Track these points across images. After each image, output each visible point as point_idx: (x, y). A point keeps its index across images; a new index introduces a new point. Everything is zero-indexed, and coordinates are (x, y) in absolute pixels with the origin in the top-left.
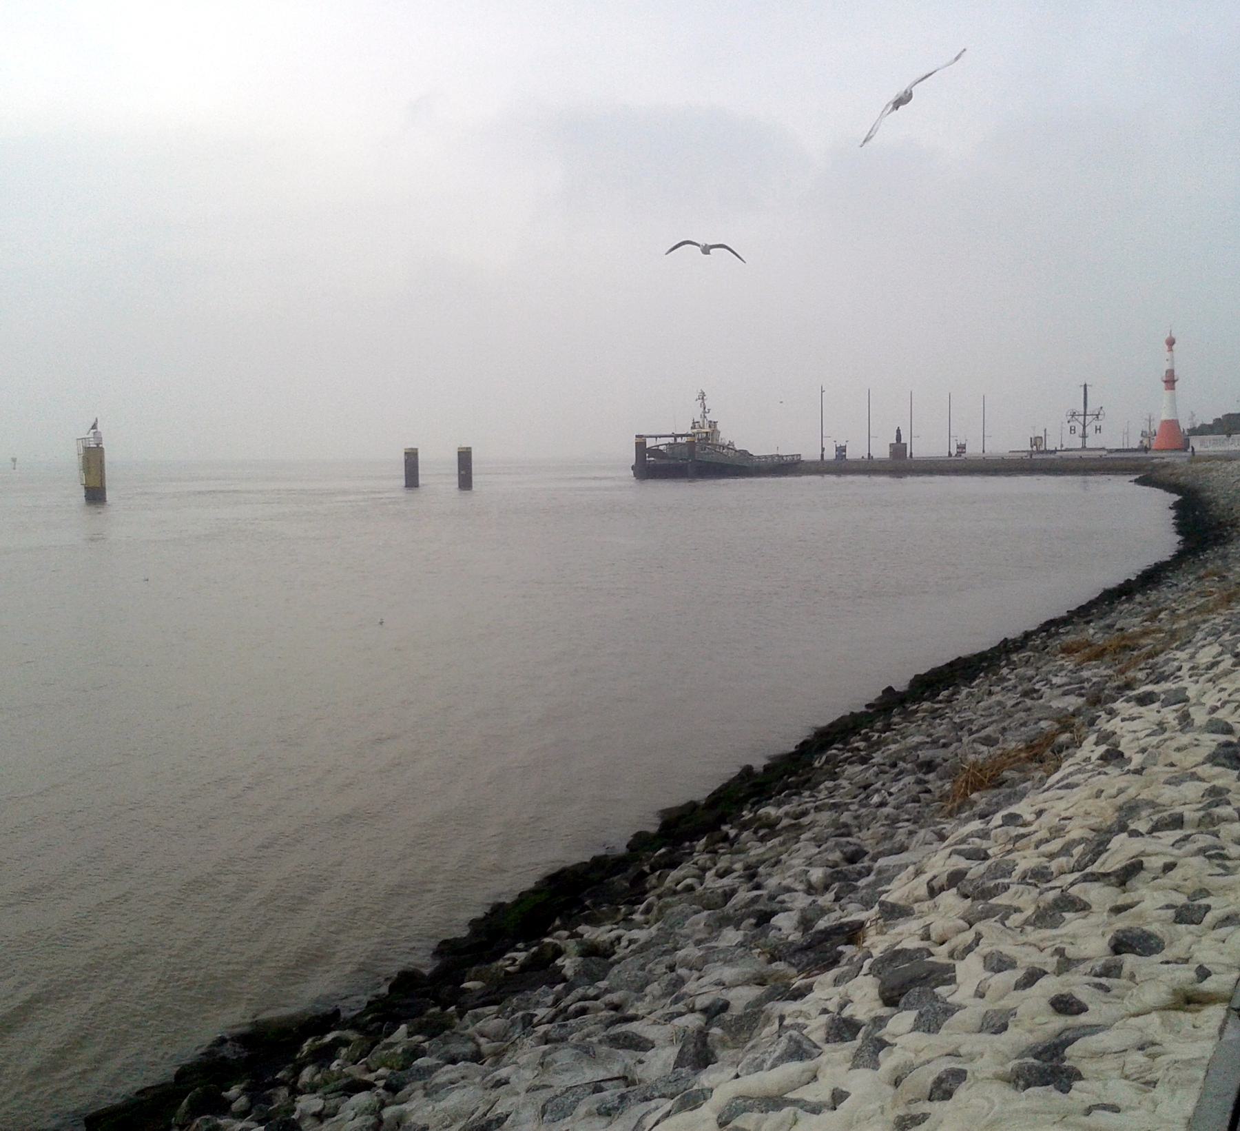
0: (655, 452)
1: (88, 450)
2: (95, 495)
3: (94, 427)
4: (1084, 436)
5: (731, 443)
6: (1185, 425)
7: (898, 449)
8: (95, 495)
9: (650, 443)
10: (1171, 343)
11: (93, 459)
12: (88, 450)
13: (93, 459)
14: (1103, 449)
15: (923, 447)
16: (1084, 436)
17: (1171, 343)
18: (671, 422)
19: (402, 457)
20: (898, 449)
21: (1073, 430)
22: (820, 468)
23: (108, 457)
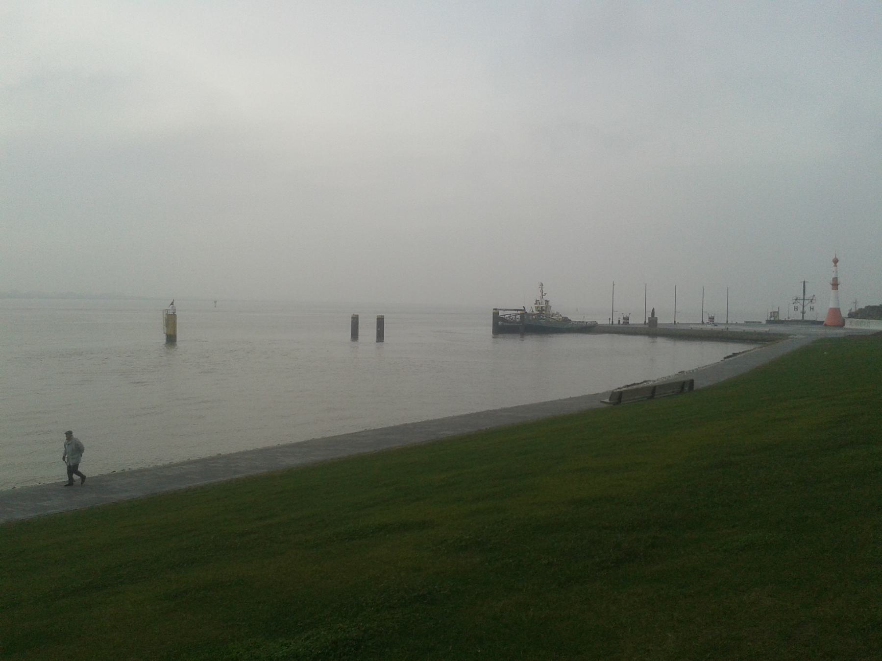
0: (503, 319)
1: (168, 315)
2: (171, 339)
3: (172, 304)
4: (803, 313)
5: (557, 313)
6: (844, 314)
7: (653, 321)
8: (171, 339)
9: (501, 313)
10: (836, 261)
11: (171, 320)
12: (168, 315)
13: (171, 320)
14: (634, 384)
15: (664, 320)
16: (803, 313)
17: (836, 261)
18: (520, 299)
19: (350, 320)
20: (653, 321)
21: (796, 309)
22: (624, 329)
23: (178, 321)
